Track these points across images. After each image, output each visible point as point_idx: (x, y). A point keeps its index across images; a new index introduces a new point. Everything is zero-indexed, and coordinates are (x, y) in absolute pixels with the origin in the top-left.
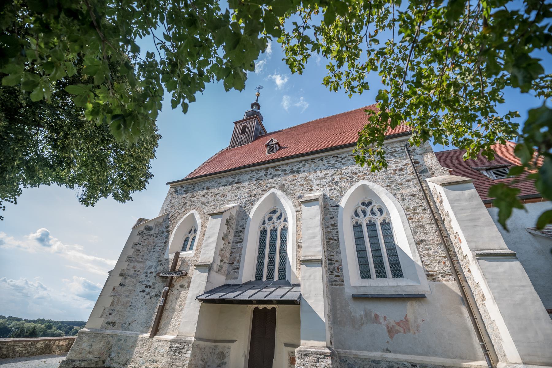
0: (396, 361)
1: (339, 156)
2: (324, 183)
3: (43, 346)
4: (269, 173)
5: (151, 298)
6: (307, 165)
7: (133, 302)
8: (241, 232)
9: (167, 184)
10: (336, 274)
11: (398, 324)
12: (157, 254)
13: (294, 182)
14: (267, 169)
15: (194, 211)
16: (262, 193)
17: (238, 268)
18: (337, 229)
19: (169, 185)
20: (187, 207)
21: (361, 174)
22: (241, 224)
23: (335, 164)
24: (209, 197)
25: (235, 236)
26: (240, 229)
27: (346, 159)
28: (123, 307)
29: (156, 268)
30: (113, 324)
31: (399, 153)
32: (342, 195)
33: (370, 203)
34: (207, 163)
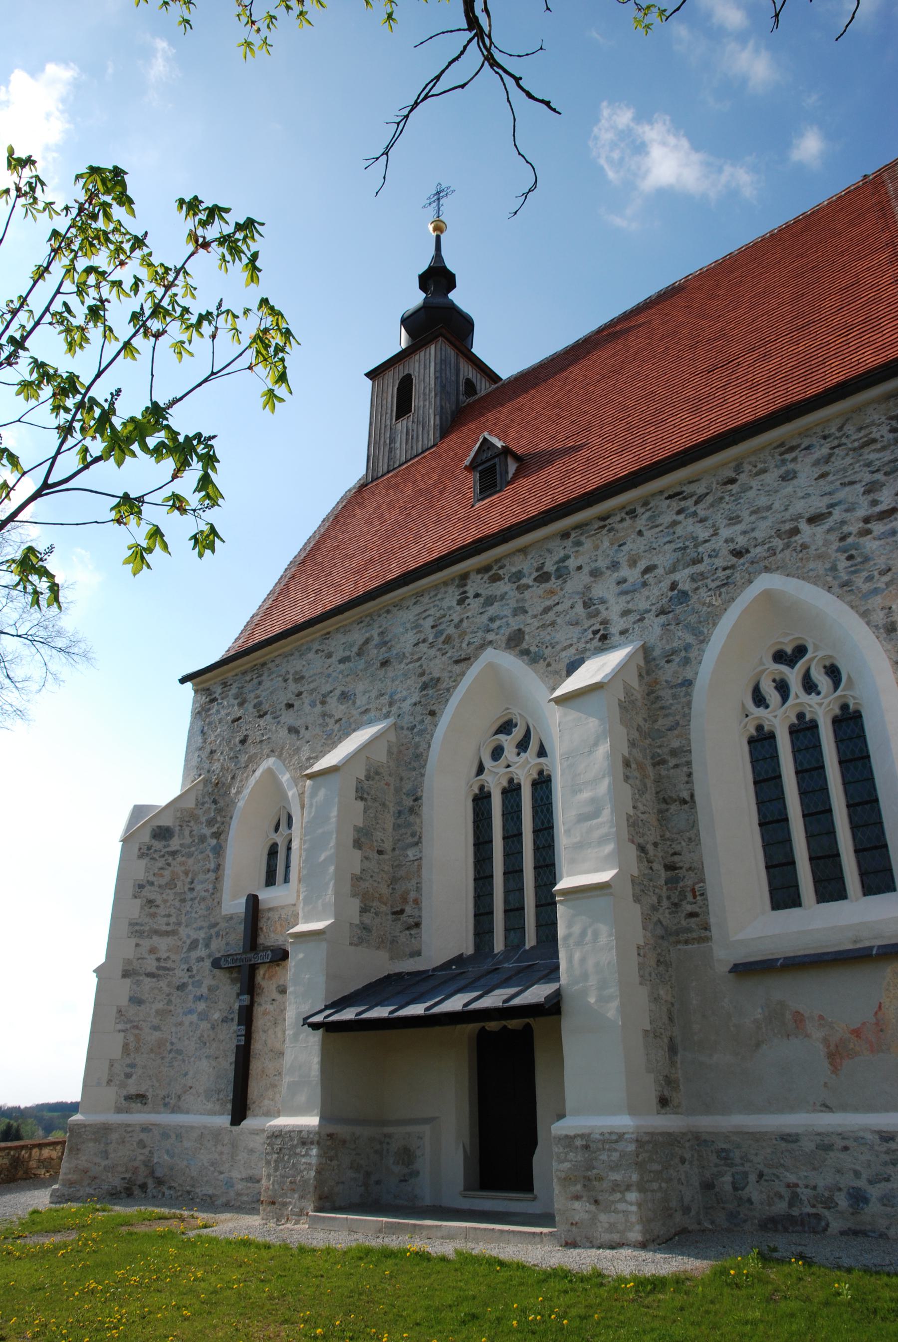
0: (840, 1130)
1: (688, 489)
2: (643, 605)
4: (471, 594)
5: (213, 1027)
6: (588, 544)
7: (174, 1040)
8: (412, 810)
9: (183, 681)
10: (689, 908)
11: (857, 1033)
12: (203, 906)
13: (551, 616)
14: (464, 578)
15: (270, 762)
16: (457, 669)
17: (417, 925)
18: (689, 763)
19: (189, 685)
20: (252, 750)
21: (759, 549)
22: (408, 786)
23: (675, 523)
24: (307, 708)
25: (396, 827)
26: (409, 802)
27: (710, 499)
28: (152, 1056)
29: (207, 946)
30: (141, 1098)
31: (884, 448)
32: (704, 640)
33: (801, 651)
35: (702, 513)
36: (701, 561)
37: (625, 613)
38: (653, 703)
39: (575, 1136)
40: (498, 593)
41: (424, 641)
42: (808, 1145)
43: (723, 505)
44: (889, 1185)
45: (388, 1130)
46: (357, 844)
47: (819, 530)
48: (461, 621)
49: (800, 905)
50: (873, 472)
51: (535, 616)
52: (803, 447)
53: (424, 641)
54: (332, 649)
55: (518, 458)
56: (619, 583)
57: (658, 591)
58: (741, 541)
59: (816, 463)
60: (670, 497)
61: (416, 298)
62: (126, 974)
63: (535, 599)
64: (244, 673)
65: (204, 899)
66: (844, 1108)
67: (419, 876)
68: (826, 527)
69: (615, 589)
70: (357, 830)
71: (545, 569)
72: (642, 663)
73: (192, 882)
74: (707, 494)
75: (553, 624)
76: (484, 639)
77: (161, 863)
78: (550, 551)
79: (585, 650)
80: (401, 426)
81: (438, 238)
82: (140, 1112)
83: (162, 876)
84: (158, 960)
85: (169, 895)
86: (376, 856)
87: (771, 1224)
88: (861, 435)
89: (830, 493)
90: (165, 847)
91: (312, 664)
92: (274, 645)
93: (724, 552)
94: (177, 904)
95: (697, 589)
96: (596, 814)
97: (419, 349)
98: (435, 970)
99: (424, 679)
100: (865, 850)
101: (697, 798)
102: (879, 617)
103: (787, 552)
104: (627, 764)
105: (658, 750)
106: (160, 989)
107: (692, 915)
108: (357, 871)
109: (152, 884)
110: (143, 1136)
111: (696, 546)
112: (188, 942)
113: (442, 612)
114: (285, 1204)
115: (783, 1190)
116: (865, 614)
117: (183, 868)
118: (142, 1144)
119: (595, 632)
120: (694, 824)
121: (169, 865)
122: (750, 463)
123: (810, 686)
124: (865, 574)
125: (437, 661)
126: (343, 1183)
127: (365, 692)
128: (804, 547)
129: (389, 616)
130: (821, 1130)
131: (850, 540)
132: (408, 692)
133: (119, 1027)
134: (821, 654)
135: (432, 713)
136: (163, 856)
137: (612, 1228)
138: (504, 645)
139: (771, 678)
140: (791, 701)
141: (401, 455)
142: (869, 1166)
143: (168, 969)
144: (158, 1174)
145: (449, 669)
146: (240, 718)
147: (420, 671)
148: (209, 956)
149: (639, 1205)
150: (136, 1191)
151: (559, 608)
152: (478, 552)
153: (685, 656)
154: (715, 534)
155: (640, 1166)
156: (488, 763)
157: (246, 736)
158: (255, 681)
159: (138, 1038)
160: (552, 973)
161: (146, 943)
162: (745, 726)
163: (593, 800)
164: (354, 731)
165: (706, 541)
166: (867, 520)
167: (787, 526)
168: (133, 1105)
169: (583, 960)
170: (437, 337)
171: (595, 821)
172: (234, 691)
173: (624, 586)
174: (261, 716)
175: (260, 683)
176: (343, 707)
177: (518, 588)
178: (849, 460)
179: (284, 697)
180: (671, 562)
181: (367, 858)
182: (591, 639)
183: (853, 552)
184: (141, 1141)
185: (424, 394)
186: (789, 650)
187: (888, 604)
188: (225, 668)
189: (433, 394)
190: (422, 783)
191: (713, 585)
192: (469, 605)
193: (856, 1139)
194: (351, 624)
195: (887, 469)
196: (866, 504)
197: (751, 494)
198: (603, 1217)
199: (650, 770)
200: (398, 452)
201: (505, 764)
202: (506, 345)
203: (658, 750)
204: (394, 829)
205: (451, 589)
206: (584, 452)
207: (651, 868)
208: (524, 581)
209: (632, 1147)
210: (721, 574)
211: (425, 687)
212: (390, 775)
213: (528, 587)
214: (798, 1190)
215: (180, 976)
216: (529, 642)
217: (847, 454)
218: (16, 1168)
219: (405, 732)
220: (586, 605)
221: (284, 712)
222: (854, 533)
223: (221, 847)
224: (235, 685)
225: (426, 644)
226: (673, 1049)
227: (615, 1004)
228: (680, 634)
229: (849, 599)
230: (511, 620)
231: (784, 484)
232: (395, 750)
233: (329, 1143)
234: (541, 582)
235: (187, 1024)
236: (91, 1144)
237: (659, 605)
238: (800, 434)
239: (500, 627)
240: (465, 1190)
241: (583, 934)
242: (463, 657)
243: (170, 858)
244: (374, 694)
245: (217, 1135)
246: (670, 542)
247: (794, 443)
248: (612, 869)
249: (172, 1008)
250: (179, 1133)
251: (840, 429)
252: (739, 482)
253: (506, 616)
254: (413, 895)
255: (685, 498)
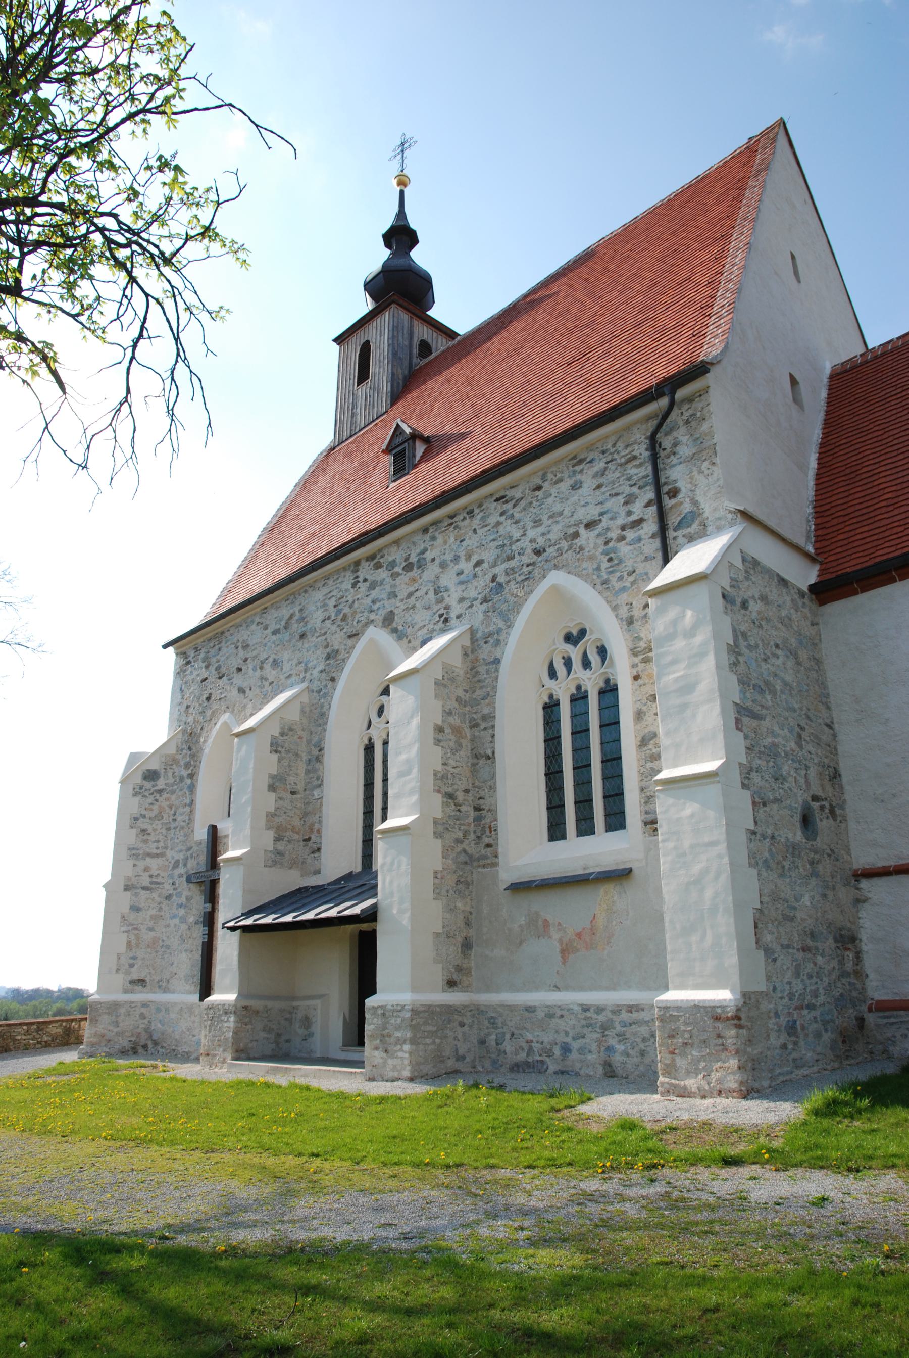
0: (559, 1004)
2: (473, 594)
3: (59, 1030)
4: (361, 579)
5: (189, 929)
6: (440, 540)
7: (165, 939)
9: (165, 647)
11: (579, 935)
14: (357, 563)
16: (350, 642)
17: (319, 850)
18: (493, 727)
20: (215, 707)
21: (552, 549)
22: (315, 739)
23: (498, 524)
24: (251, 672)
25: (308, 772)
26: (315, 752)
27: (523, 503)
28: (149, 950)
29: (185, 865)
30: (141, 982)
31: (641, 465)
34: (276, 529)
35: (517, 516)
36: (513, 558)
37: (461, 600)
38: (474, 677)
39: (378, 1007)
40: (379, 579)
41: (329, 618)
42: (541, 1014)
43: (532, 509)
44: (584, 1041)
45: (295, 1004)
46: (272, 788)
47: (593, 534)
48: (354, 602)
49: (594, 833)
50: (631, 486)
51: (402, 600)
52: (588, 460)
53: (329, 618)
54: (268, 622)
55: (426, 440)
56: (458, 574)
57: (483, 582)
58: (541, 541)
59: (595, 476)
60: (497, 500)
61: (380, 255)
62: (127, 888)
63: (403, 585)
64: (210, 640)
65: (183, 828)
66: (567, 988)
67: (321, 811)
68: (596, 532)
69: (456, 580)
70: (272, 777)
71: (411, 560)
72: (468, 643)
73: (175, 814)
74: (522, 498)
75: (413, 607)
76: (368, 618)
77: (150, 799)
78: (414, 544)
79: (434, 630)
80: (362, 391)
81: (402, 193)
82: (141, 992)
83: (152, 810)
84: (151, 876)
85: (158, 824)
86: (290, 796)
87: (516, 1068)
88: (627, 452)
89: (601, 503)
90: (153, 786)
91: (254, 635)
92: (227, 618)
93: (529, 551)
94: (164, 831)
95: (509, 582)
96: (408, 772)
97: (383, 310)
98: (329, 884)
99: (328, 650)
100: (610, 796)
101: (496, 755)
102: (624, 612)
103: (570, 552)
104: (440, 730)
105: (475, 716)
106: (153, 899)
107: (489, 846)
108: (272, 810)
109: (144, 816)
110: (143, 1010)
111: (511, 545)
112: (173, 862)
113: (341, 593)
114: (215, 1055)
115: (524, 1045)
116: (615, 608)
117: (168, 803)
118: (142, 1016)
119: (441, 616)
120: (493, 776)
121: (157, 801)
122: (552, 472)
123: (586, 664)
124: (618, 574)
125: (337, 636)
126: (256, 1041)
127: (289, 660)
128: (581, 549)
129: (306, 595)
130: (549, 1004)
131: (611, 545)
132: (317, 661)
133: (124, 929)
134: (594, 637)
135: (333, 680)
136: (152, 794)
137: (394, 1068)
138: (381, 624)
139: (561, 656)
140: (572, 676)
141: (361, 421)
142: (574, 1028)
143: (159, 884)
144: (154, 1038)
146: (206, 679)
147: (325, 643)
148: (186, 873)
149: (410, 1053)
150: (140, 1050)
151: (418, 594)
152: (363, 544)
153: (495, 638)
154: (524, 535)
155: (414, 1028)
156: (375, 719)
157: (210, 694)
158: (217, 647)
159: (138, 937)
160: (372, 890)
161: (141, 864)
163: (408, 761)
164: (281, 692)
165: (518, 541)
166: (623, 528)
167: (571, 531)
168: (136, 987)
169: (391, 882)
170: (390, 304)
171: (408, 778)
172: (202, 655)
173: (462, 577)
174: (220, 678)
175: (220, 649)
176: (274, 672)
177: (392, 575)
178: (617, 474)
179: (236, 662)
180: (493, 557)
181: (280, 799)
182: (438, 622)
183: (612, 555)
184: (142, 1013)
185: (380, 361)
186: (575, 633)
187: (630, 601)
188: (208, 629)
189: (386, 361)
190: (324, 737)
191: (519, 579)
193: (568, 1010)
194: (281, 601)
195: (641, 483)
196: (623, 514)
197: (550, 500)
198: (390, 1061)
199: (468, 732)
200: (358, 417)
201: (385, 721)
202: (459, 306)
203: (475, 716)
204: (306, 773)
205: (348, 573)
206: (467, 442)
207: (459, 810)
208: (397, 569)
209: (408, 1015)
210: (525, 569)
211: (328, 657)
212: (303, 730)
213: (398, 574)
214: (533, 1045)
215: (167, 888)
216: (398, 622)
217: (616, 469)
218: (68, 1035)
219: (315, 694)
220: (436, 592)
221: (235, 675)
222: (614, 538)
223: (194, 786)
224: (202, 651)
225: (330, 621)
226: (467, 945)
227: (407, 915)
228: (495, 620)
229: (605, 594)
230: (386, 603)
231: (573, 492)
232: (307, 709)
233: (244, 1012)
234: (407, 571)
235: (172, 925)
236: (106, 1017)
237: (483, 595)
238: (587, 448)
239: (379, 608)
240: (344, 1046)
241: (392, 863)
243: (158, 796)
244: (295, 662)
245: (190, 1008)
246: (494, 540)
247: (582, 457)
248: (721, 758)
249: (162, 913)
250: (166, 1008)
251: (614, 445)
252: (543, 490)
253: (383, 599)
254: (316, 826)
255: (507, 502)
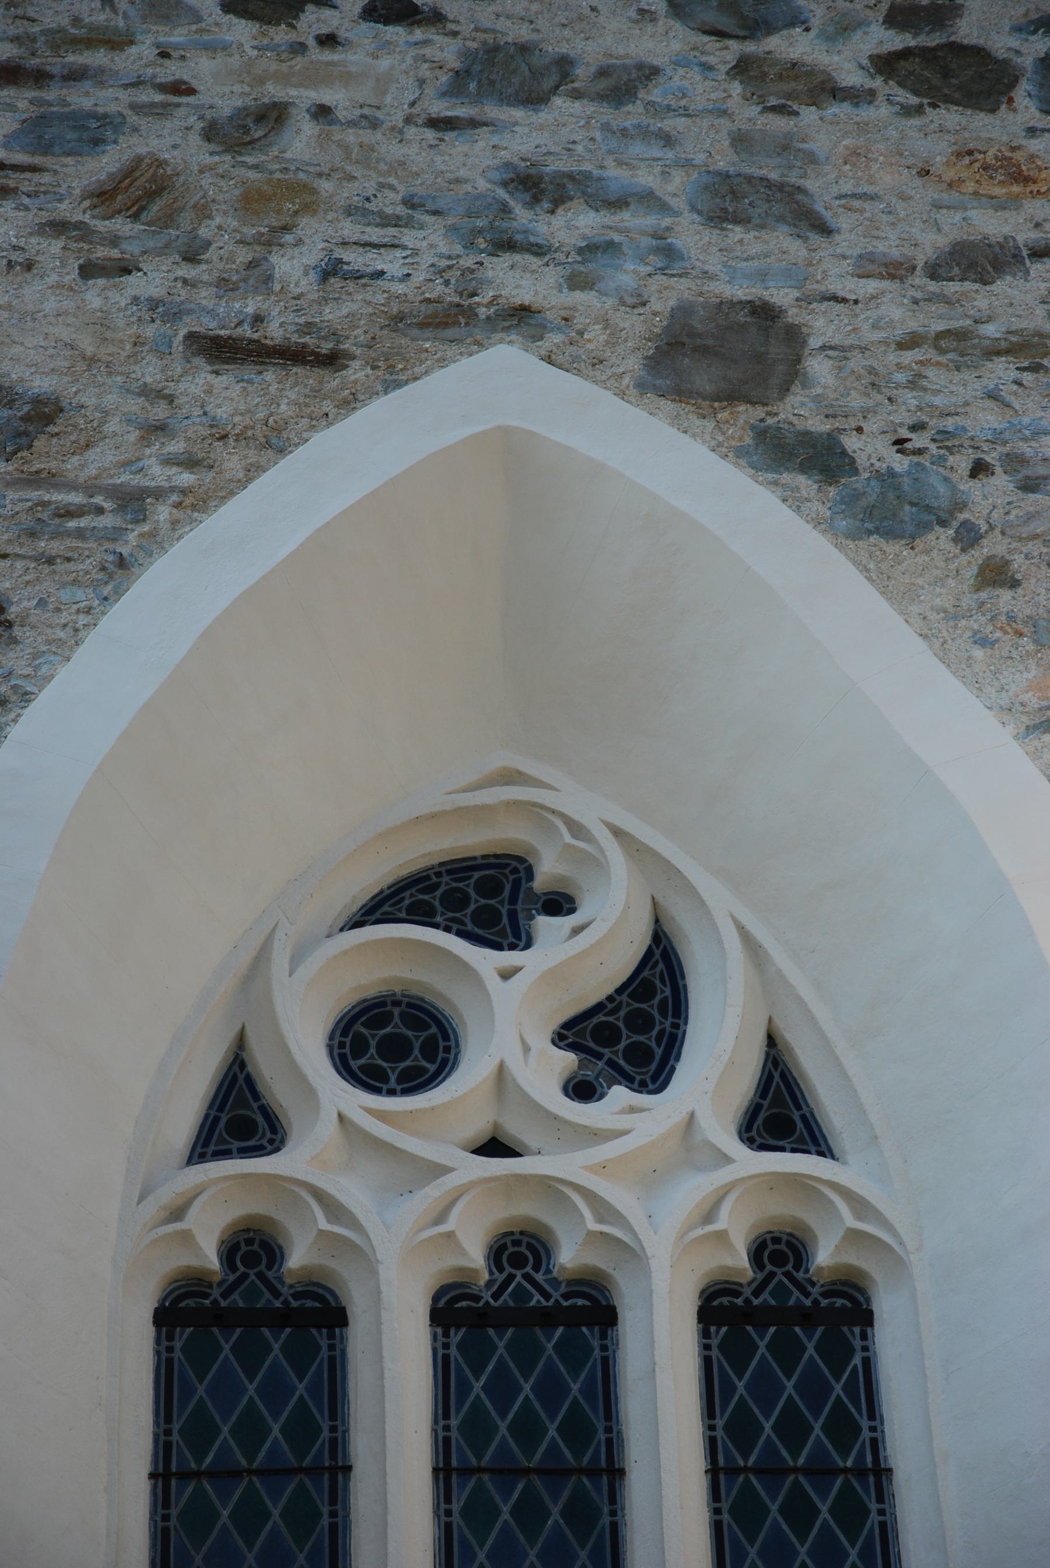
16: (225, 394)
138: (633, 364)
145: (150, 372)
162: (177, 1213)
192: (328, 41)
213: (826, 90)
230: (691, 236)
242: (275, 332)
